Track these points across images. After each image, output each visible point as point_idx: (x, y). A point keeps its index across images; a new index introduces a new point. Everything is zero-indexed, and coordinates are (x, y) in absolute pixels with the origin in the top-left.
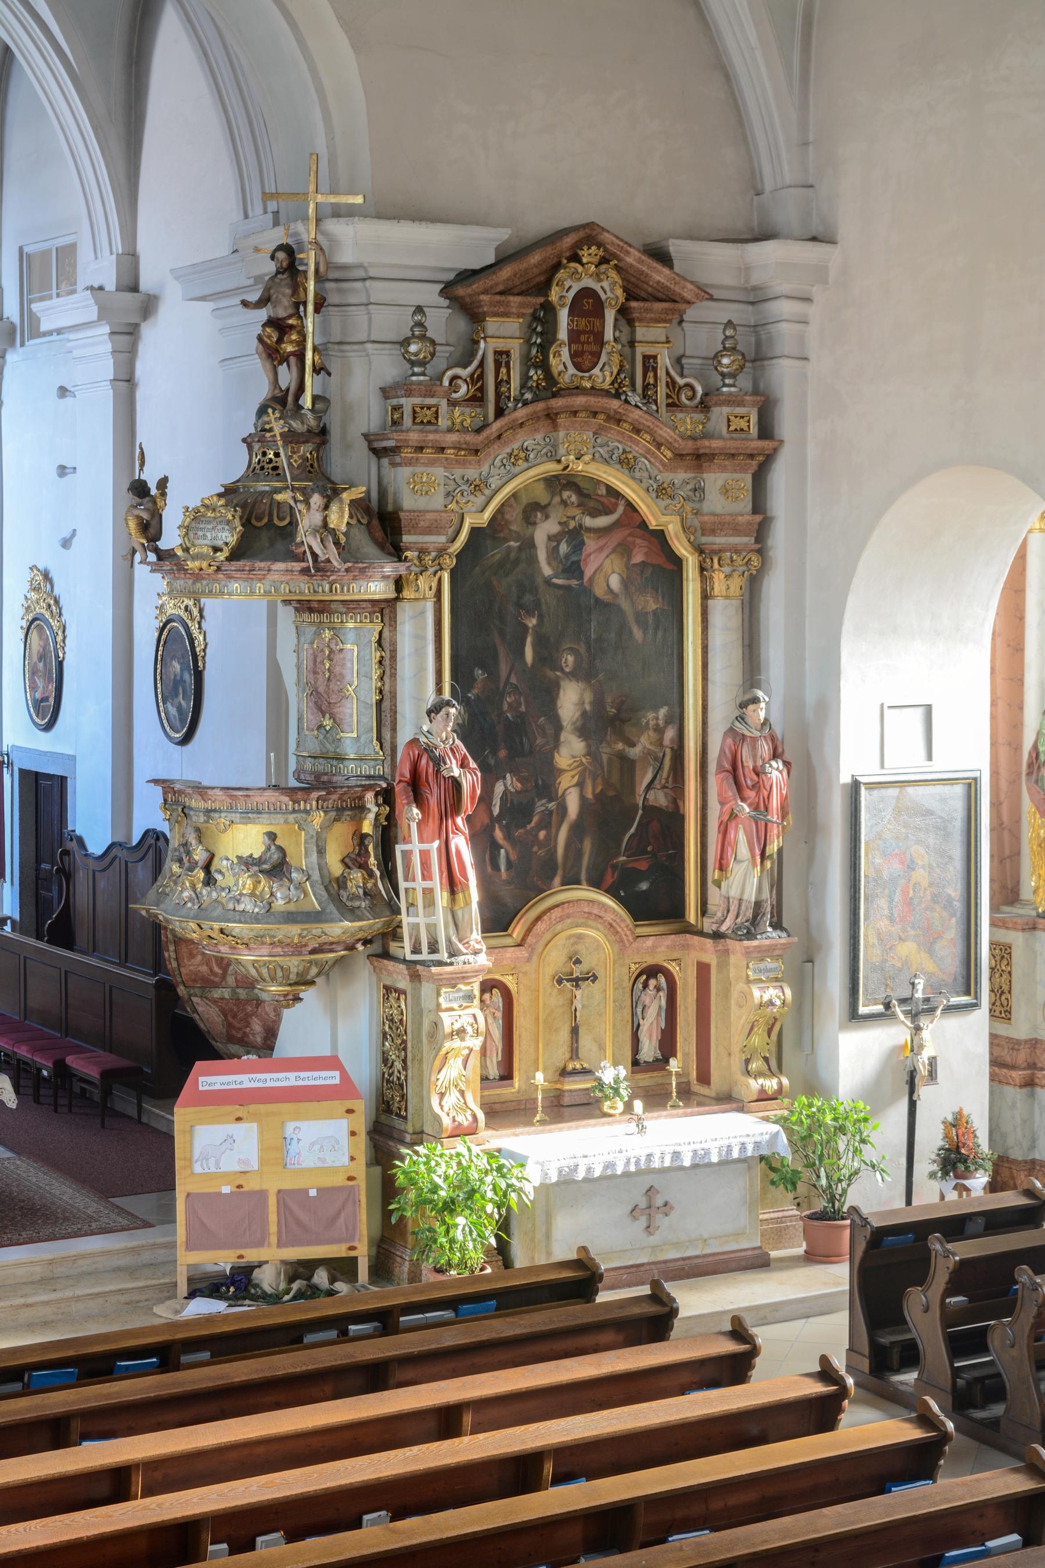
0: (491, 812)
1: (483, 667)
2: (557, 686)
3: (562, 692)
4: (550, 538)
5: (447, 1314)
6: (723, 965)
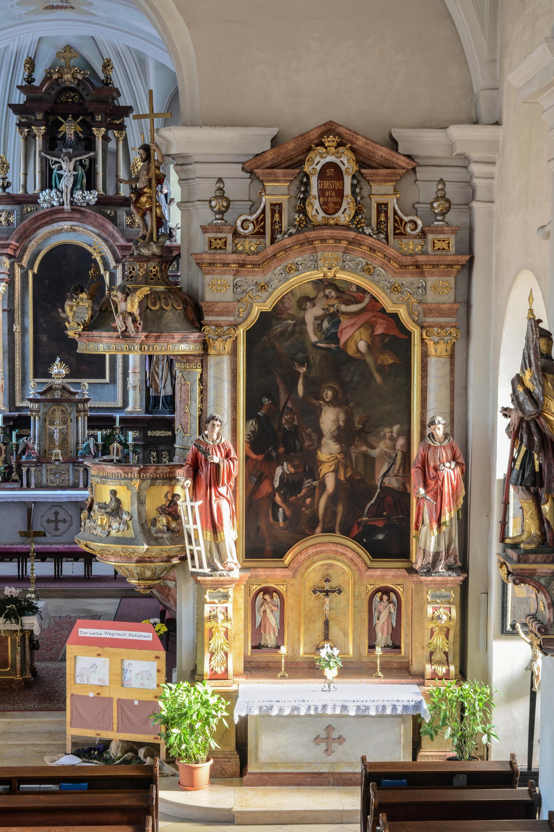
0: (273, 486)
1: (270, 397)
2: (321, 410)
3: (323, 413)
4: (316, 318)
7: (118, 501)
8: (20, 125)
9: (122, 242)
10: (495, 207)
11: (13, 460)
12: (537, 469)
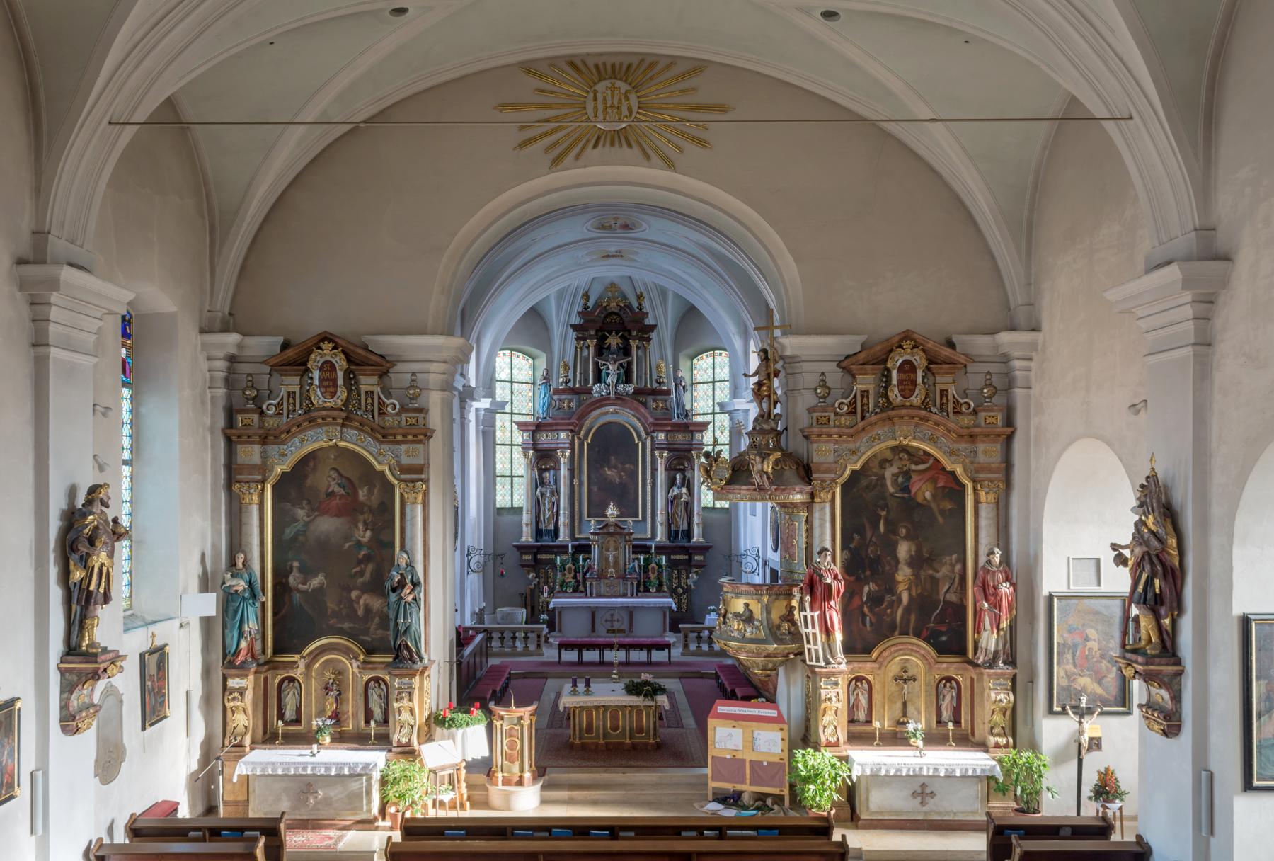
1: (858, 533)
5: (753, 833)
6: (980, 679)
7: (751, 611)
8: (578, 339)
9: (651, 420)
10: (1032, 392)
11: (580, 577)
12: (1157, 591)
